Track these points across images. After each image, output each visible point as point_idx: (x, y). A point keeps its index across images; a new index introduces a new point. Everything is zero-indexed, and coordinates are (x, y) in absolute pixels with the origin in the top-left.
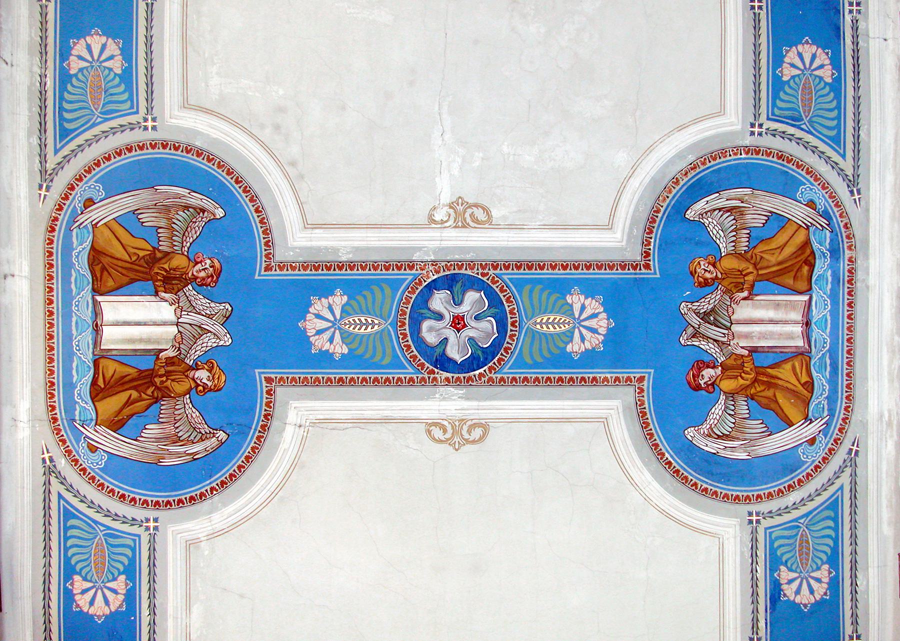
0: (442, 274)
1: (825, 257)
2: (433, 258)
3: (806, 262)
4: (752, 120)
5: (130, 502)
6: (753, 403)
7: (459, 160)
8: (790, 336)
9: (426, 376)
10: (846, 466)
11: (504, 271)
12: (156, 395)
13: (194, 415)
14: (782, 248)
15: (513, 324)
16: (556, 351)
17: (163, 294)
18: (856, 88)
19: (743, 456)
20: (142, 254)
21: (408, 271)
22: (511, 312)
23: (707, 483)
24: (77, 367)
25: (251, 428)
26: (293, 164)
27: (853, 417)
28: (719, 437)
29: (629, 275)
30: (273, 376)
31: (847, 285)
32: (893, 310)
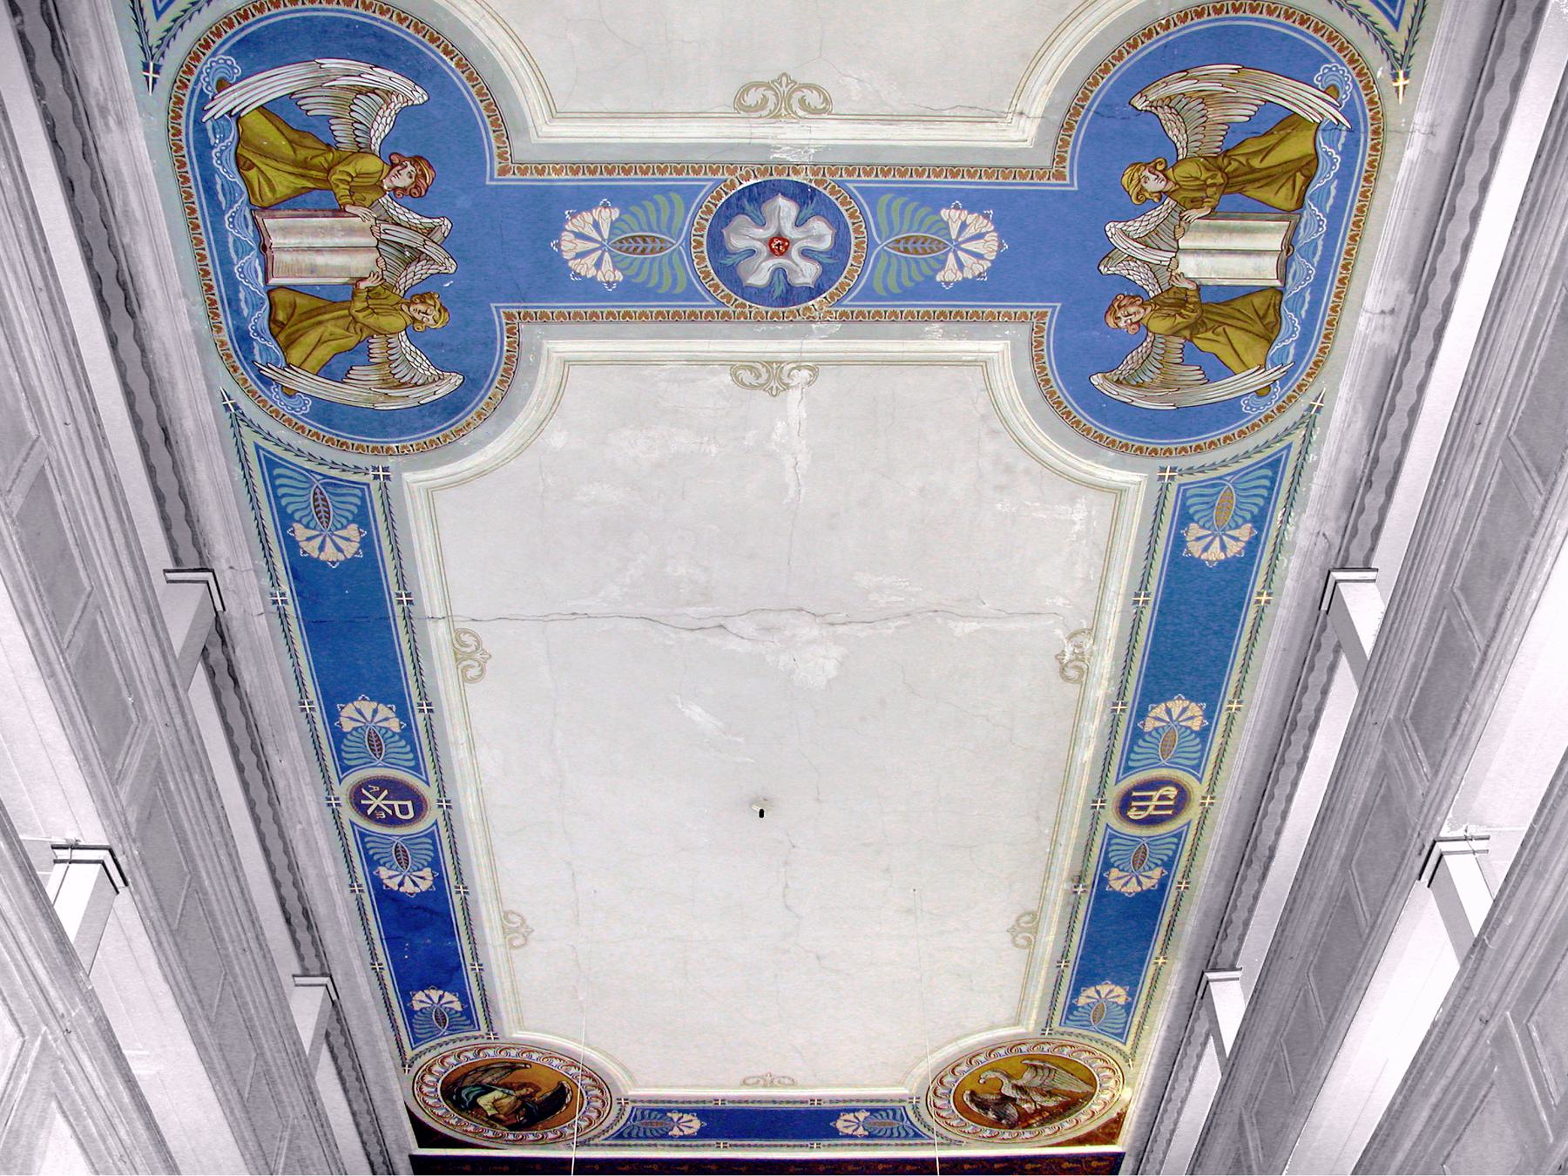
0: (801, 307)
1: (255, 331)
2: (814, 326)
3: (282, 326)
4: (388, 483)
5: (1294, 13)
6: (326, 138)
7: (774, 436)
8: (285, 231)
9: (828, 178)
10: (158, 47)
11: (714, 310)
12: (1226, 161)
13: (1176, 131)
14: (320, 342)
15: (700, 244)
16: (634, 209)
17: (1190, 286)
18: (259, 518)
19: (329, 63)
20: (1209, 335)
21: (848, 310)
22: (702, 259)
23: (383, 22)
24: (1328, 198)
25: (1096, 112)
26: (994, 432)
27: (164, 119)
28: (373, 91)
29: (534, 308)
30: (1053, 181)
31: (217, 298)
32: (140, 268)
